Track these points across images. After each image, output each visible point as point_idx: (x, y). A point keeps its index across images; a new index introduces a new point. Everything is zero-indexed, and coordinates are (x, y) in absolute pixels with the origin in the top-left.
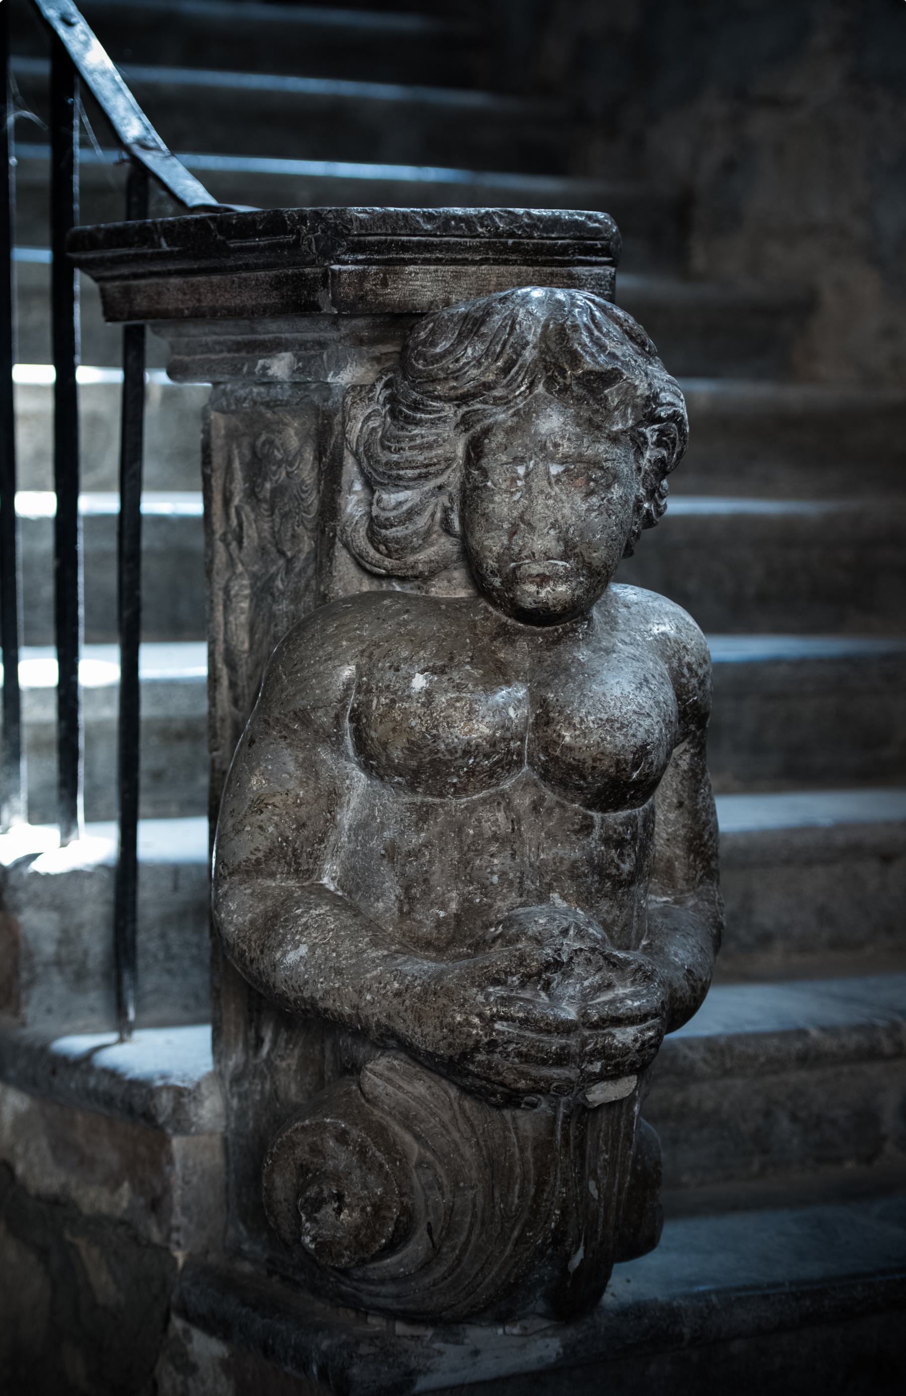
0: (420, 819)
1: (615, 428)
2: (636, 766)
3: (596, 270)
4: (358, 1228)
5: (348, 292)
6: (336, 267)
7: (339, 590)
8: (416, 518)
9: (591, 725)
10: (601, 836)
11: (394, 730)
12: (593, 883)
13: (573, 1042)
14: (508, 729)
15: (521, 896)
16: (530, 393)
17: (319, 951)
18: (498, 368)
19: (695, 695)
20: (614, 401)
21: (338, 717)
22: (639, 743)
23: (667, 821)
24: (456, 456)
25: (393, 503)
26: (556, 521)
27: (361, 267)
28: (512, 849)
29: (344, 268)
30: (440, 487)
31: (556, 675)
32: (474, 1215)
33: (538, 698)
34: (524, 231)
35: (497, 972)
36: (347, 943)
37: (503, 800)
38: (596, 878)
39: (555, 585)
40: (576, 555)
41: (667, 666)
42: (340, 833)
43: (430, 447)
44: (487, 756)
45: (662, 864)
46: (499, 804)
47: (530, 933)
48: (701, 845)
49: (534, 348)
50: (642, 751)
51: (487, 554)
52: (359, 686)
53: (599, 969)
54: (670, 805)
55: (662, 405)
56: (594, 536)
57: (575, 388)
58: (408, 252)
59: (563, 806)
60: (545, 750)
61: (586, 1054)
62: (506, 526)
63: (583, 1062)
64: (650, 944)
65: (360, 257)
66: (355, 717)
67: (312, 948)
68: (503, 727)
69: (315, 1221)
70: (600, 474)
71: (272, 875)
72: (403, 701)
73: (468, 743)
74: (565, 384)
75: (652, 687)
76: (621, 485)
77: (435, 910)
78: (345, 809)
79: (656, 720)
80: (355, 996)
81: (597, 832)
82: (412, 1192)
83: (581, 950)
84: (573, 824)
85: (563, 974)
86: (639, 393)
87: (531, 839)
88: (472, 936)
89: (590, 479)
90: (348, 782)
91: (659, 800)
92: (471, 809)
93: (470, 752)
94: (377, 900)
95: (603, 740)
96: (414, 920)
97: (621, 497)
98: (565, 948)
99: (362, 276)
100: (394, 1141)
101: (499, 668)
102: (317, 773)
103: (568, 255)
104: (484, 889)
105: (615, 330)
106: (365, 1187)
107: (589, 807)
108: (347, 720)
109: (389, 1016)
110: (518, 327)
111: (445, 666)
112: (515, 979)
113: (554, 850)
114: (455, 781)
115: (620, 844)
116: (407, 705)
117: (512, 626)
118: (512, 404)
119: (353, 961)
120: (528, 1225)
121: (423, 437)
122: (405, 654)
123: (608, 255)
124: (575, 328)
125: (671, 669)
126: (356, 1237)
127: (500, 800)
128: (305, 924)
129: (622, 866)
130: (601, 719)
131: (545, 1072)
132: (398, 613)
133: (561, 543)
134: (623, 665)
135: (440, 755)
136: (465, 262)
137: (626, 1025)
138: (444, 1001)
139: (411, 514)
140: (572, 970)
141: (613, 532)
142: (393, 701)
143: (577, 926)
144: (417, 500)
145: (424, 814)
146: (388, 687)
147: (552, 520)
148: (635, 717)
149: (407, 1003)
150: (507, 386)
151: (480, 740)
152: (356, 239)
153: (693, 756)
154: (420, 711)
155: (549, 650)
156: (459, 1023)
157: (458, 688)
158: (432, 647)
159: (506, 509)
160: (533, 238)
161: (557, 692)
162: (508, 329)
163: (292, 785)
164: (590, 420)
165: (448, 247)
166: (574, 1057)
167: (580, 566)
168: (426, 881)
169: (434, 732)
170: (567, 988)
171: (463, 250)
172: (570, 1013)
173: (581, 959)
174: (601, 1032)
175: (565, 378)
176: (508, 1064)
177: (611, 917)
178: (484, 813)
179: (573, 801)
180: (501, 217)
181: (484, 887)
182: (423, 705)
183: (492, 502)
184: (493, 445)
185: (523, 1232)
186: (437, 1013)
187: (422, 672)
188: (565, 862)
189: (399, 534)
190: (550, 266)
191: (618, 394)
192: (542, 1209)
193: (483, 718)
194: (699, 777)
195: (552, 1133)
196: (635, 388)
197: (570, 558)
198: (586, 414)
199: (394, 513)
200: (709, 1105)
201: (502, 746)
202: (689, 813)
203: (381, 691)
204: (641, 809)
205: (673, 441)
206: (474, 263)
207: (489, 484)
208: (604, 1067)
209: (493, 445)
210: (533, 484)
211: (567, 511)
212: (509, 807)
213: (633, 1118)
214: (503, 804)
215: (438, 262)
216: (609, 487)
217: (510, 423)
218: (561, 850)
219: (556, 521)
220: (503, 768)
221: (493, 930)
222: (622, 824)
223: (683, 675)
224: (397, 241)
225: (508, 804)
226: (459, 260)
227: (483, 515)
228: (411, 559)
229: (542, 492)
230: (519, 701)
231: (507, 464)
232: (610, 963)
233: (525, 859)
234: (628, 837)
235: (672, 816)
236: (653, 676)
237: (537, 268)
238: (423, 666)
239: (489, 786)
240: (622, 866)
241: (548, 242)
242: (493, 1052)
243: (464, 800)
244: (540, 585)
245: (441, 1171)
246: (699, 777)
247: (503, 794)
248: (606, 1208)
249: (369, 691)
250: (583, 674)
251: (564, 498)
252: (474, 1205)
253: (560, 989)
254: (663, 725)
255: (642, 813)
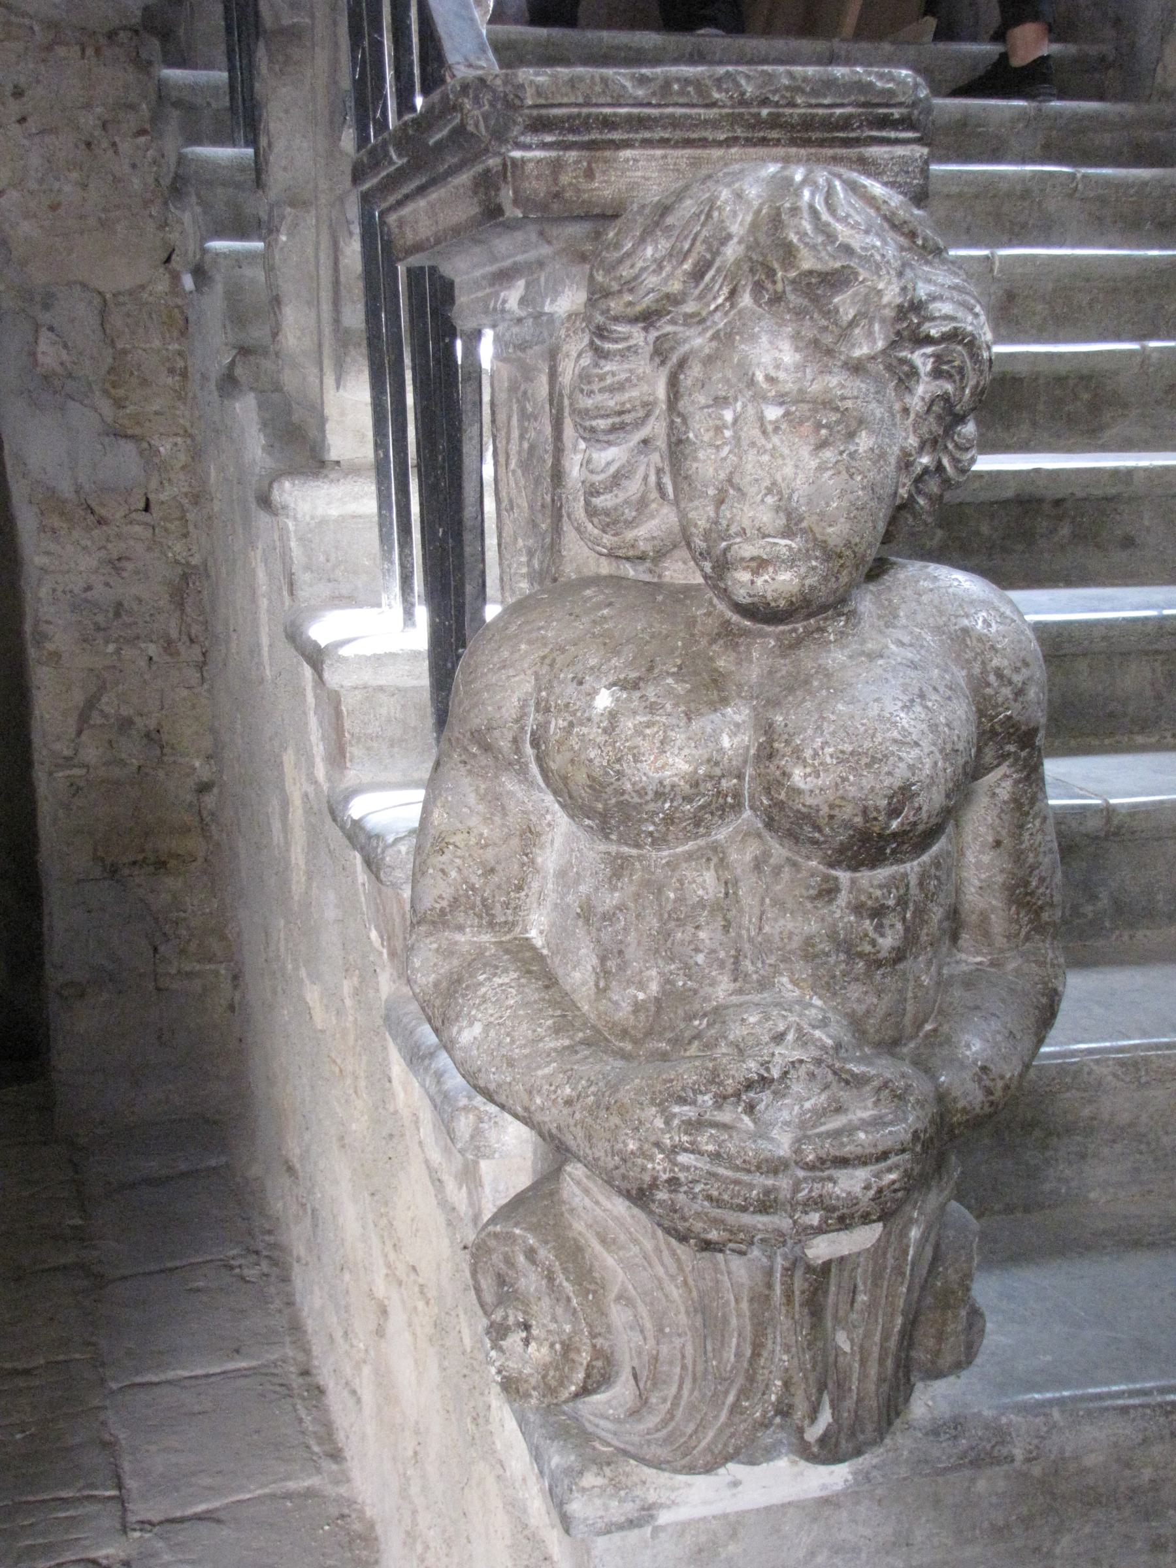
0: (614, 875)
1: (856, 353)
2: (894, 813)
3: (900, 151)
4: (546, 1367)
5: (537, 187)
6: (517, 154)
7: (570, 571)
8: (625, 483)
9: (828, 760)
10: (849, 903)
11: (572, 761)
12: (837, 963)
13: (784, 1183)
14: (717, 764)
15: (735, 980)
16: (732, 306)
17: (492, 1033)
18: (685, 273)
19: (1008, 709)
20: (848, 313)
21: (515, 740)
22: (897, 783)
23: (979, 865)
24: (656, 399)
25: (603, 462)
26: (774, 484)
27: (553, 154)
28: (725, 919)
29: (529, 154)
30: (645, 442)
31: (791, 690)
32: (684, 1367)
33: (763, 722)
34: (783, 97)
35: (683, 1089)
36: (525, 1026)
37: (716, 855)
38: (842, 957)
39: (775, 572)
40: (803, 531)
41: (964, 673)
42: (544, 878)
43: (620, 387)
44: (688, 799)
45: (974, 917)
46: (709, 860)
47: (731, 1037)
48: (1027, 894)
49: (739, 243)
50: (904, 794)
51: (693, 530)
52: (538, 704)
53: (827, 1087)
54: (983, 845)
55: (934, 319)
56: (828, 504)
57: (791, 297)
58: (616, 129)
59: (795, 864)
60: (768, 791)
61: (798, 1203)
62: (711, 492)
63: (795, 1211)
64: (935, 1030)
65: (549, 139)
66: (535, 744)
67: (488, 1026)
68: (709, 761)
69: (501, 1350)
70: (834, 417)
71: (460, 928)
72: (582, 724)
73: (661, 783)
74: (776, 292)
75: (930, 704)
76: (872, 431)
77: (632, 991)
78: (548, 851)
79: (926, 751)
80: (525, 1097)
81: (843, 898)
82: (609, 1332)
83: (801, 1061)
84: (807, 889)
85: (775, 1093)
86: (885, 300)
87: (751, 907)
88: (673, 1029)
89: (819, 426)
90: (549, 817)
91: (970, 839)
92: (672, 865)
93: (664, 794)
94: (574, 968)
95: (844, 779)
96: (610, 999)
97: (872, 449)
98: (777, 1059)
99: (557, 166)
100: (592, 1265)
101: (715, 681)
102: (503, 808)
103: (853, 130)
104: (688, 969)
105: (860, 213)
106: (554, 1319)
107: (831, 865)
108: (528, 745)
109: (559, 1128)
110: (716, 214)
111: (640, 678)
112: (706, 1098)
113: (782, 922)
114: (651, 828)
115: (878, 912)
116: (585, 730)
117: (737, 624)
118: (709, 323)
119: (526, 1051)
120: (744, 1393)
121: (614, 374)
122: (593, 662)
123: (912, 127)
124: (795, 211)
125: (970, 676)
126: (544, 1377)
127: (710, 854)
128: (484, 996)
129: (880, 940)
130: (842, 752)
131: (747, 1219)
132: (599, 606)
133: (781, 514)
134: (889, 676)
135: (626, 797)
136: (704, 143)
137: (854, 1166)
138: (615, 1120)
139: (617, 480)
140: (788, 1087)
141: (858, 498)
142: (571, 725)
143: (799, 1029)
144: (624, 460)
145: (618, 868)
146: (567, 705)
147: (767, 483)
148: (894, 748)
149: (578, 1116)
150: (701, 297)
151: (676, 779)
152: (535, 112)
153: (1017, 782)
154: (601, 739)
155: (783, 656)
156: (632, 1153)
157: (652, 708)
158: (629, 652)
159: (711, 470)
160: (795, 105)
161: (787, 714)
162: (703, 218)
163: (474, 821)
164: (816, 342)
165: (675, 123)
166: (783, 1204)
167: (810, 545)
168: (620, 952)
169: (617, 767)
170: (780, 1110)
171: (696, 126)
172: (782, 1143)
173: (803, 1070)
174: (819, 1174)
175: (774, 282)
176: (696, 1207)
177: (864, 1007)
178: (688, 871)
179: (808, 858)
180: (748, 77)
181: (687, 966)
182: (605, 731)
183: (696, 459)
184: (689, 382)
185: (738, 1400)
186: (608, 1135)
187: (608, 687)
188: (796, 938)
189: (609, 504)
190: (830, 147)
191: (853, 303)
192: (760, 1378)
193: (680, 749)
194: (1026, 808)
195: (770, 1286)
196: (879, 293)
197: (795, 535)
198: (809, 333)
199: (601, 477)
200: (1125, 1118)
201: (709, 785)
202: (1010, 855)
203: (560, 711)
204: (915, 863)
205: (961, 370)
206: (719, 144)
207: (691, 435)
208: (824, 1220)
209: (689, 382)
210: (743, 434)
211: (789, 470)
212: (723, 864)
213: (908, 1246)
214: (715, 860)
215: (664, 143)
216: (851, 435)
217: (707, 351)
218: (788, 923)
219: (774, 484)
220: (712, 814)
221: (697, 1023)
222: (880, 887)
223: (988, 685)
224: (597, 116)
225: (722, 860)
226: (694, 140)
227: (686, 478)
228: (630, 535)
229: (753, 444)
230: (737, 725)
231: (708, 407)
232: (841, 1080)
233: (744, 932)
234: (891, 902)
235: (986, 859)
236: (935, 689)
237: (813, 150)
238: (611, 679)
239: (697, 836)
240: (880, 940)
241: (820, 111)
242: (676, 1191)
243: (666, 853)
244: (756, 572)
245: (643, 1310)
246: (1026, 808)
247: (715, 848)
248: (863, 1362)
249: (547, 710)
250: (828, 689)
251: (786, 451)
252: (683, 1357)
253: (771, 1110)
254: (938, 756)
255: (917, 869)
